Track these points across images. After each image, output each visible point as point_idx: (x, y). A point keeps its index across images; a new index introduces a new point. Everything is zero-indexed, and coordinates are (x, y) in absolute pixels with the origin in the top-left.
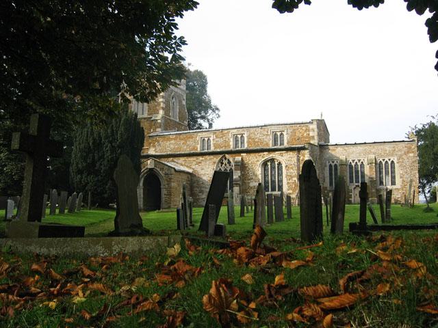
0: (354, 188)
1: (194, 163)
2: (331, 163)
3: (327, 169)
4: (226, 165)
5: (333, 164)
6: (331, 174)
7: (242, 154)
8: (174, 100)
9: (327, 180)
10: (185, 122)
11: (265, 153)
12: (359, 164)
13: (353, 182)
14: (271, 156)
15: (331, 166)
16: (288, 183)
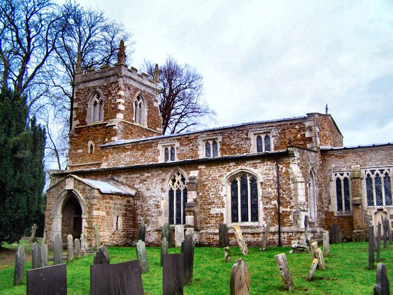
0: (376, 213)
1: (138, 181)
2: (338, 175)
3: (333, 185)
4: (178, 183)
5: (342, 178)
6: (339, 193)
7: (199, 167)
8: (141, 101)
9: (334, 201)
10: (158, 129)
11: (232, 164)
12: (382, 176)
13: (373, 204)
14: (240, 167)
15: (338, 180)
16: (265, 209)
